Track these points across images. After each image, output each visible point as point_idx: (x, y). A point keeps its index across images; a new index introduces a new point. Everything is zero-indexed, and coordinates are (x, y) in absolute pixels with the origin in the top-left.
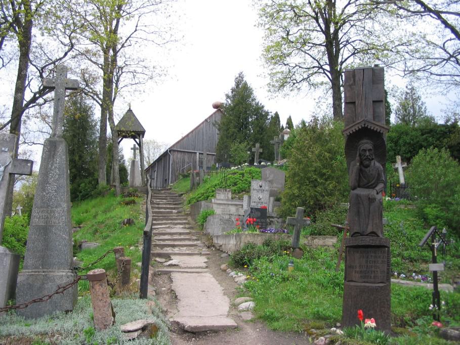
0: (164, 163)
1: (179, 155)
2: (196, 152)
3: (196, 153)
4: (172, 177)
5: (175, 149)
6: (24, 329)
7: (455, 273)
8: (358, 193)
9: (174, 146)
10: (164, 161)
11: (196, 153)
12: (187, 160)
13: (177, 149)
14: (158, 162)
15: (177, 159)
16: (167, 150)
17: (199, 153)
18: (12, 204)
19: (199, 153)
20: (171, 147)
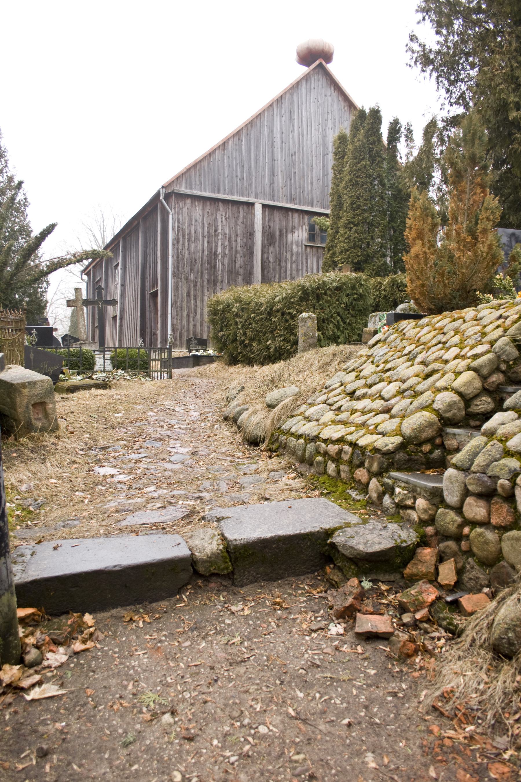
0: (146, 246)
1: (198, 211)
2: (251, 200)
3: (253, 204)
4: (176, 288)
5: (183, 189)
6: (279, 162)
7: (151, 429)
8: (461, 453)
9: (178, 179)
10: (145, 233)
11: (253, 204)
12: (223, 227)
13: (188, 192)
14: (125, 239)
15: (190, 225)
16: (158, 195)
17: (264, 206)
18: (428, 468)
19: (264, 206)
20: (171, 184)
